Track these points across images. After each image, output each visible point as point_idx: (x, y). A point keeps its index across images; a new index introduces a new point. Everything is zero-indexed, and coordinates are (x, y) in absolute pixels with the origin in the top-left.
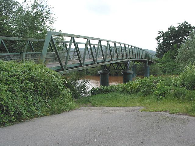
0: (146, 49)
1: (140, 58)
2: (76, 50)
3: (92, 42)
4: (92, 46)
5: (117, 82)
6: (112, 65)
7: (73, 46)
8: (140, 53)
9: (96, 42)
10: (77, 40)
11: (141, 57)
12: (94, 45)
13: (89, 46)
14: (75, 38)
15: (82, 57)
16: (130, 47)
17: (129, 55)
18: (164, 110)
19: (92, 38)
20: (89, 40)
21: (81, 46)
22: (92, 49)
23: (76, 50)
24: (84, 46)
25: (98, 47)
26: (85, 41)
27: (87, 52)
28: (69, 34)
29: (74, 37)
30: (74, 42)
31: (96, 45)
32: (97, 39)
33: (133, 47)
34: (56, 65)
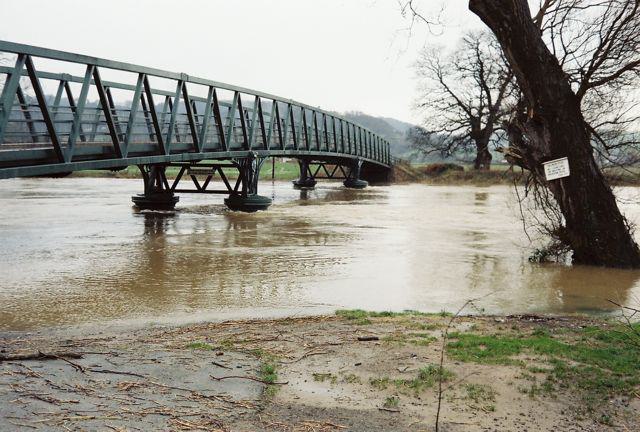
1: (336, 151)
2: (105, 108)
6: (202, 184)
7: (93, 95)
8: (372, 145)
10: (105, 75)
11: (369, 154)
12: (64, 81)
14: (100, 69)
18: (36, 352)
19: (109, 65)
20: (96, 70)
21: (122, 98)
23: (105, 108)
24: (130, 95)
26: (132, 79)
28: (46, 49)
29: (28, 55)
30: (97, 82)
32: (229, 88)
34: (339, 219)
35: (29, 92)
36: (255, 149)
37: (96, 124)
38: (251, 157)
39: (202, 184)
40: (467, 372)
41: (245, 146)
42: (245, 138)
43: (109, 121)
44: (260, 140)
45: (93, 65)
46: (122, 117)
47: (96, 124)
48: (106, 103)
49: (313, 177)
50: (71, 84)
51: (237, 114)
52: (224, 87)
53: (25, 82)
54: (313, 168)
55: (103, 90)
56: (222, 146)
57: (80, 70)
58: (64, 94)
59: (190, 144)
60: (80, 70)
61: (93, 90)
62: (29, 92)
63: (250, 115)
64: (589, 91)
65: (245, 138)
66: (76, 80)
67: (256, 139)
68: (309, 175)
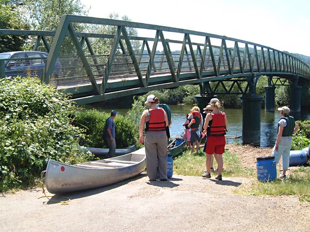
0: (298, 55)
1: (43, 72)
3: (194, 39)
4: (195, 48)
5: (31, 188)
6: (236, 84)
7: (160, 48)
9: (202, 40)
10: (167, 35)
12: (199, 45)
13: (187, 46)
15: (177, 64)
16: (242, 46)
17: (283, 66)
21: (175, 48)
22: (195, 53)
25: (205, 49)
26: (181, 37)
27: (185, 56)
30: (163, 40)
31: (202, 45)
33: (249, 46)
35: (188, 49)
36: (254, 72)
37: (162, 62)
38: (253, 76)
39: (236, 84)
40: (280, 163)
41: (251, 70)
42: (215, 68)
43: (168, 61)
44: (263, 68)
45: (159, 30)
46: (175, 58)
47: (162, 62)
48: (167, 51)
49: (274, 85)
50: (149, 42)
51: (224, 51)
52: (230, 39)
53: (187, 46)
54: (274, 79)
55: (166, 43)
56: (241, 71)
57: (152, 34)
58: (146, 48)
59: (238, 70)
60: (152, 34)
61: (160, 45)
62: (188, 49)
63: (232, 53)
64: (287, 171)
65: (215, 68)
66: (151, 39)
67: (255, 67)
68: (272, 84)
